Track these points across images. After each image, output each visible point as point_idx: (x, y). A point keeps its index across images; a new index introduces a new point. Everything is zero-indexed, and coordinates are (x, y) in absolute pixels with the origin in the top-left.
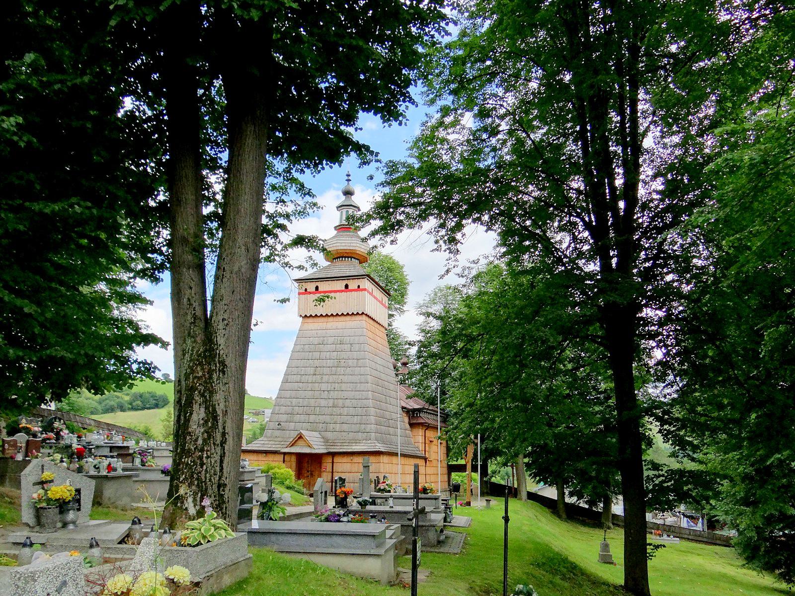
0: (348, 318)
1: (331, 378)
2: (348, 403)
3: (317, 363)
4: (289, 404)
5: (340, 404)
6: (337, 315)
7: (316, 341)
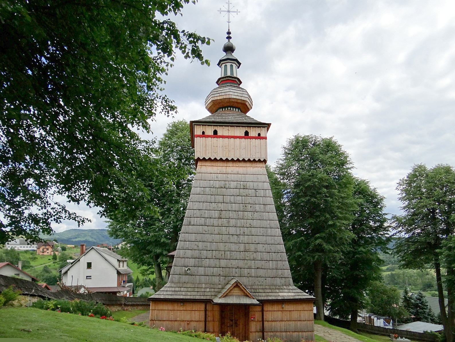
0: (248, 164)
1: (239, 223)
2: (260, 247)
3: (222, 206)
4: (196, 247)
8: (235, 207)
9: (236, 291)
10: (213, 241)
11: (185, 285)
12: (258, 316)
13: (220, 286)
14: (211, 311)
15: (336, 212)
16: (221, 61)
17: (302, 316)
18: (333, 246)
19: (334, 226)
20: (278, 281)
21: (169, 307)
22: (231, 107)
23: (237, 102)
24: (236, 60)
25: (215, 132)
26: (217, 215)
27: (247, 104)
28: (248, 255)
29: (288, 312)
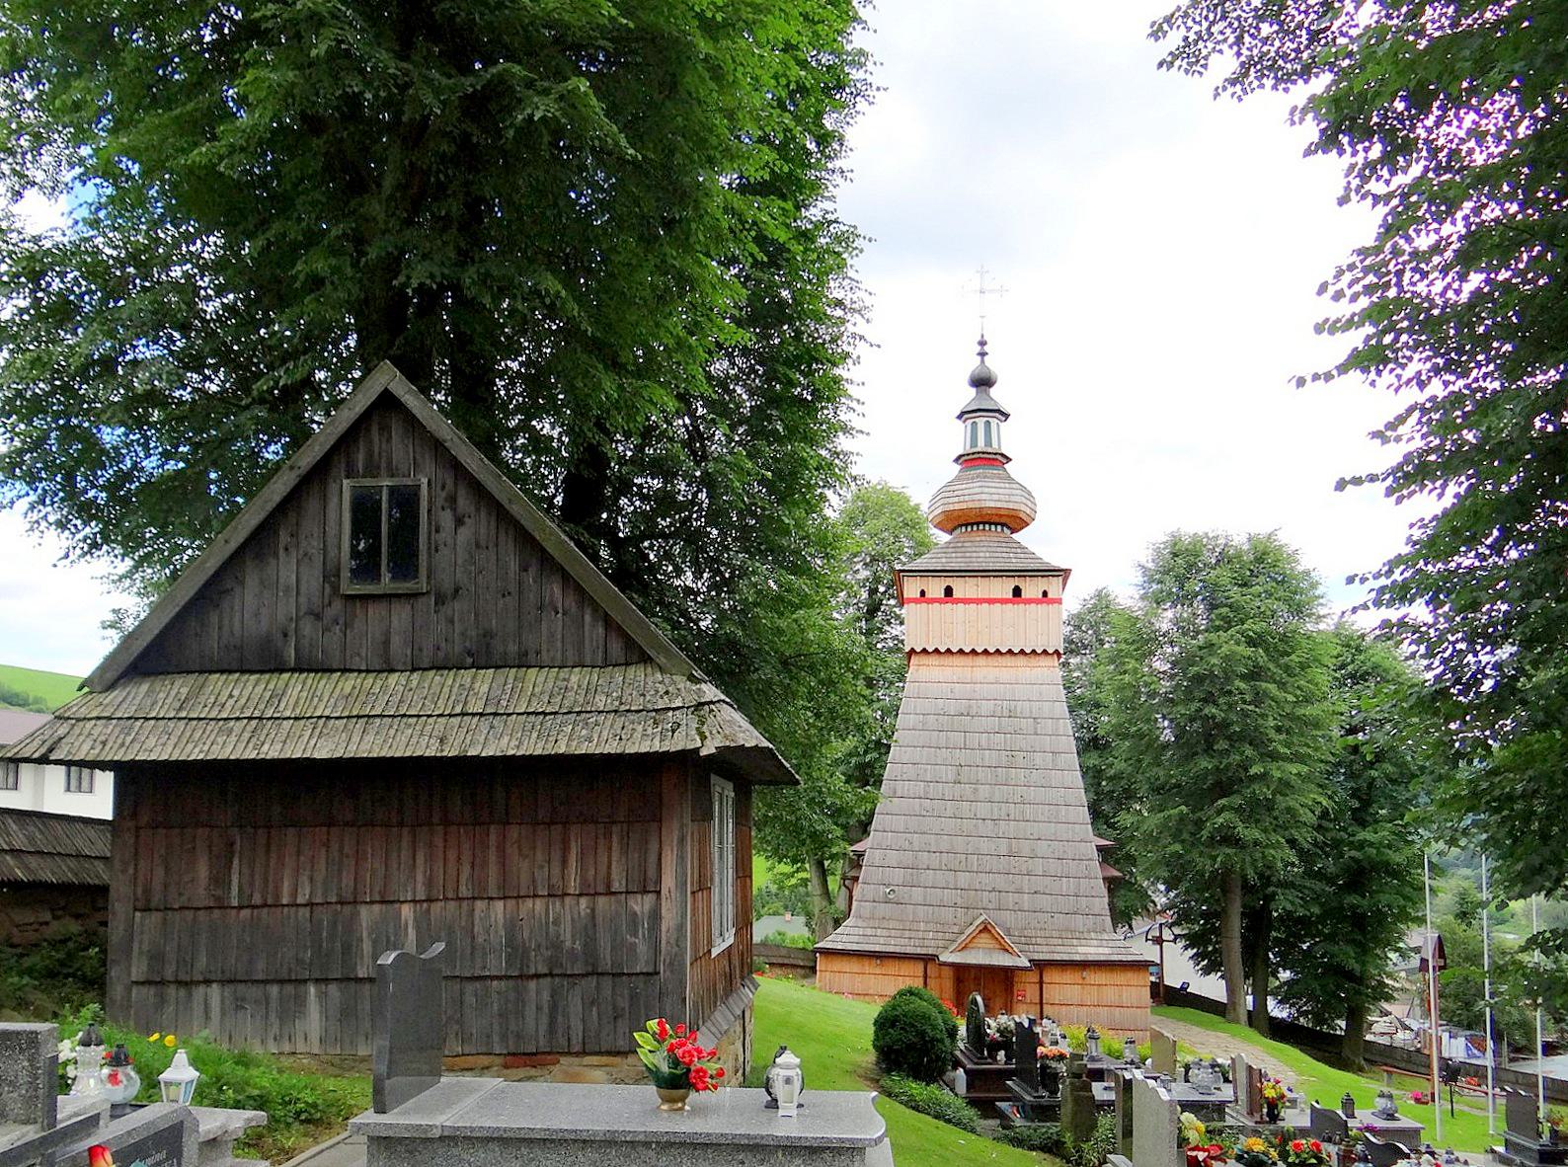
0: (1021, 660)
1: (999, 793)
2: (1043, 848)
3: (961, 756)
5: (1026, 851)
6: (986, 652)
7: (953, 707)
9: (985, 939)
11: (885, 924)
12: (1031, 993)
13: (956, 929)
15: (1271, 741)
18: (1265, 831)
19: (1263, 777)
20: (1079, 921)
21: (853, 966)
22: (984, 523)
25: (949, 591)
26: (951, 777)
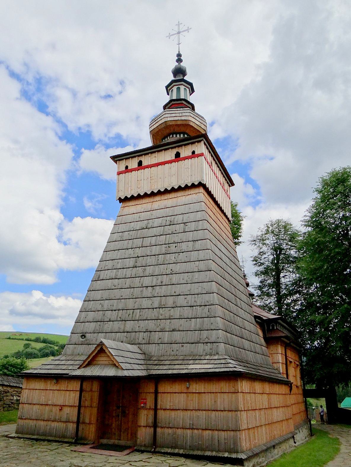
4: (99, 308)
8: (155, 250)
10: (121, 298)
12: (150, 401)
14: (89, 391)
16: (167, 87)
17: (219, 403)
23: (178, 125)
24: (191, 84)
27: (191, 124)
28: (163, 313)
29: (197, 394)
